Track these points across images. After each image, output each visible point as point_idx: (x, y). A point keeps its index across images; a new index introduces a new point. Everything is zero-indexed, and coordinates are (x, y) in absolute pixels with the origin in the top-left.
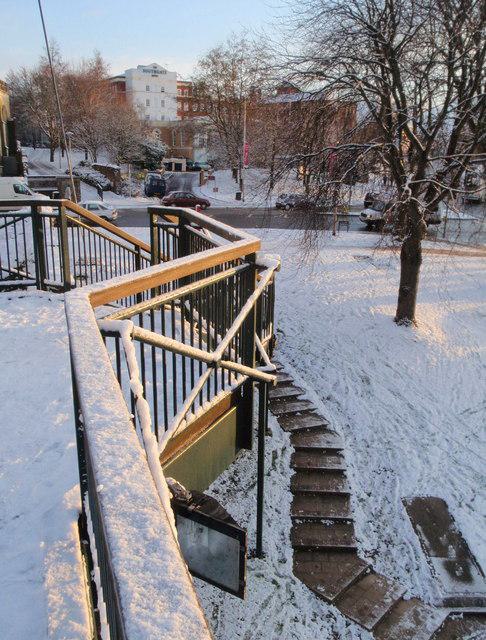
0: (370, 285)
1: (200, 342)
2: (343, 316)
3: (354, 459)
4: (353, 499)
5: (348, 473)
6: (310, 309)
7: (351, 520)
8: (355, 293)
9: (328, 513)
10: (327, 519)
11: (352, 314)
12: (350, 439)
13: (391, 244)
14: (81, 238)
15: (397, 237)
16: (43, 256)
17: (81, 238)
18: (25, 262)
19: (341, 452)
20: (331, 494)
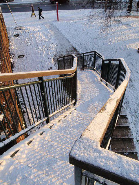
0: (124, 34)
1: (70, 98)
2: (117, 50)
3: (132, 120)
4: (135, 140)
5: (131, 127)
6: (104, 46)
7: (136, 152)
8: (119, 39)
9: (126, 149)
10: (126, 152)
11: (120, 48)
12: (128, 110)
13: (126, 15)
14: (61, 91)
15: (129, 11)
16: (117, 108)
17: (61, 91)
18: (127, 108)
19: (126, 117)
20: (126, 139)
